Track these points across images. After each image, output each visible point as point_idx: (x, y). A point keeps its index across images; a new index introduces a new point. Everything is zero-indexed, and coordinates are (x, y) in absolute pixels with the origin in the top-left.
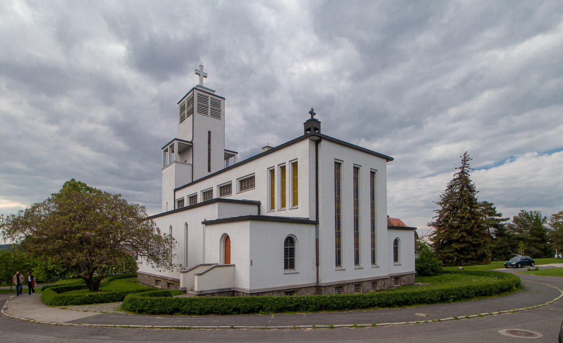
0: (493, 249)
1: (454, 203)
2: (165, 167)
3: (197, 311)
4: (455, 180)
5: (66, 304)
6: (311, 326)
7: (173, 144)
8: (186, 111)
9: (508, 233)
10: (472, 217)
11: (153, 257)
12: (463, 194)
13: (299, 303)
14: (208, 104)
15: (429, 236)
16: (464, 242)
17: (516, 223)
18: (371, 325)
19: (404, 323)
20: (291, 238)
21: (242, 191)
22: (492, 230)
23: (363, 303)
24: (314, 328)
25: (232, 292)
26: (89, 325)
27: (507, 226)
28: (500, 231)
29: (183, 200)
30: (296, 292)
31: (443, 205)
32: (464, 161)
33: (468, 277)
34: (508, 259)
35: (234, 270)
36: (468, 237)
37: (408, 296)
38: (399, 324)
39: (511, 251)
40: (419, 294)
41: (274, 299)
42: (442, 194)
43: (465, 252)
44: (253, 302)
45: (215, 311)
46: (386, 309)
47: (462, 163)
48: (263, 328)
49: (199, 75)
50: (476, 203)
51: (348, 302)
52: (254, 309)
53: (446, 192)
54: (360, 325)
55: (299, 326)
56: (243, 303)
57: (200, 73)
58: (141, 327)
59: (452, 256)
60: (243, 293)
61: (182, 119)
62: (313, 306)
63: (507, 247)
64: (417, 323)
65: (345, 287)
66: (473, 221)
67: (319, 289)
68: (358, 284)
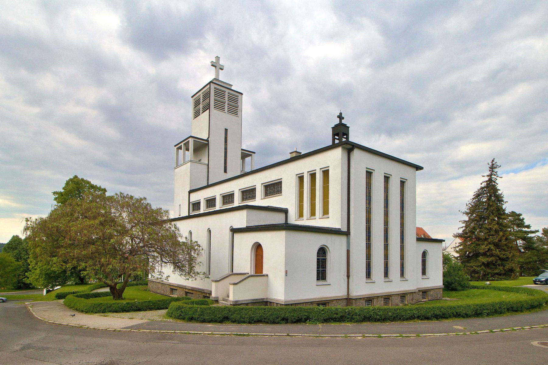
0: (521, 263)
1: (481, 213)
2: (178, 166)
3: (247, 320)
4: (482, 188)
5: (104, 312)
6: (361, 335)
7: (189, 141)
8: (201, 106)
9: (538, 247)
10: (500, 228)
11: (178, 266)
12: (491, 204)
13: (343, 314)
14: (225, 99)
15: (455, 248)
16: (492, 255)
17: (545, 236)
18: (415, 335)
19: (444, 334)
20: (323, 249)
21: (268, 197)
22: (520, 242)
23: (404, 315)
24: (364, 337)
25: (265, 302)
26: (149, 331)
27: (535, 238)
28: (528, 244)
29: (199, 203)
30: (327, 304)
31: (470, 215)
32: (492, 169)
33: (497, 292)
34: (537, 275)
35: (267, 281)
36: (496, 250)
37: (445, 309)
38: (440, 335)
39: (540, 266)
40: (455, 308)
41: (320, 310)
42: (468, 203)
43: (493, 267)
44: (300, 312)
45: (264, 320)
46: (425, 322)
47: (490, 171)
48: (318, 336)
49: (215, 67)
50: (504, 214)
51: (390, 314)
52: (302, 319)
53: (472, 201)
54: (405, 335)
55: (350, 335)
56: (290, 312)
57: (216, 65)
58: (201, 334)
59: (479, 269)
60: (277, 303)
61: (197, 114)
62: (358, 317)
63: (536, 261)
64: (456, 334)
65: (375, 300)
66: (501, 233)
67: (350, 301)
68: (387, 298)
